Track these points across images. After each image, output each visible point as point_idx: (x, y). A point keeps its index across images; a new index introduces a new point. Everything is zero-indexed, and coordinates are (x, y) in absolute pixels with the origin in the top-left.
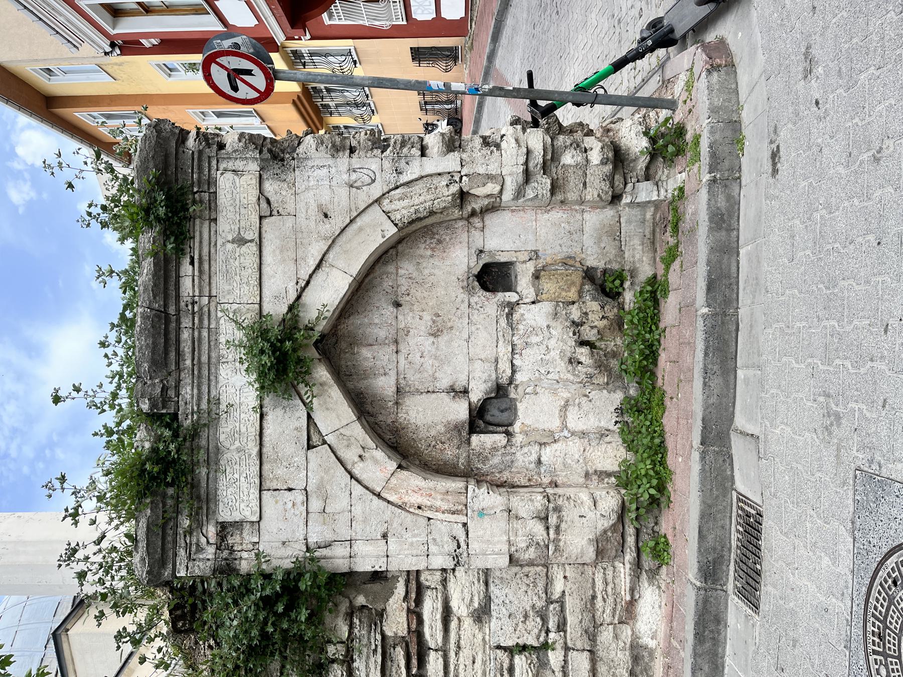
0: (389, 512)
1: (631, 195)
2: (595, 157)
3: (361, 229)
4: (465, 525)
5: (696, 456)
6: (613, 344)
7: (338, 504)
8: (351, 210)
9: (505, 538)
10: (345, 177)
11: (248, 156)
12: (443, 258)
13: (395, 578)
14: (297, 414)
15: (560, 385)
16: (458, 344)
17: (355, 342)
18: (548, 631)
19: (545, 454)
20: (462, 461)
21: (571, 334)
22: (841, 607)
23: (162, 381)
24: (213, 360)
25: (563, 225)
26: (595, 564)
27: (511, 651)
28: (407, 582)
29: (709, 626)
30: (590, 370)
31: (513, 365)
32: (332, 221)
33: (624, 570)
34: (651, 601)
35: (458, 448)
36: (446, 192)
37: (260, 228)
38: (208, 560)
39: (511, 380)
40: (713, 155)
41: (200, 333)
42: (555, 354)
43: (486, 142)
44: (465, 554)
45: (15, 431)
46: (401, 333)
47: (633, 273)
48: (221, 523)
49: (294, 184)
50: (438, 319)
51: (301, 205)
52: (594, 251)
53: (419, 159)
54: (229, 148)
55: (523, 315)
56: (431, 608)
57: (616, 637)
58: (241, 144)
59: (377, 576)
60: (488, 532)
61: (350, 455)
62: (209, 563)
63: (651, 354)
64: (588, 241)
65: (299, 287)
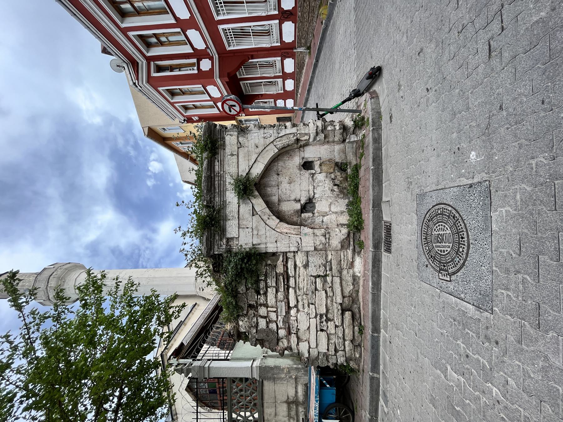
2: (337, 128)
3: (267, 151)
5: (371, 211)
7: (262, 232)
13: (279, 255)
17: (266, 186)
18: (327, 271)
22: (414, 237)
26: (341, 250)
27: (316, 277)
28: (283, 256)
29: (377, 263)
33: (350, 252)
34: (358, 262)
36: (293, 139)
39: (314, 197)
40: (373, 122)
42: (327, 188)
43: (304, 124)
45: (149, 259)
47: (350, 163)
51: (250, 144)
54: (228, 128)
56: (290, 264)
57: (348, 273)
59: (274, 254)
61: (265, 218)
63: (356, 187)
64: (336, 154)
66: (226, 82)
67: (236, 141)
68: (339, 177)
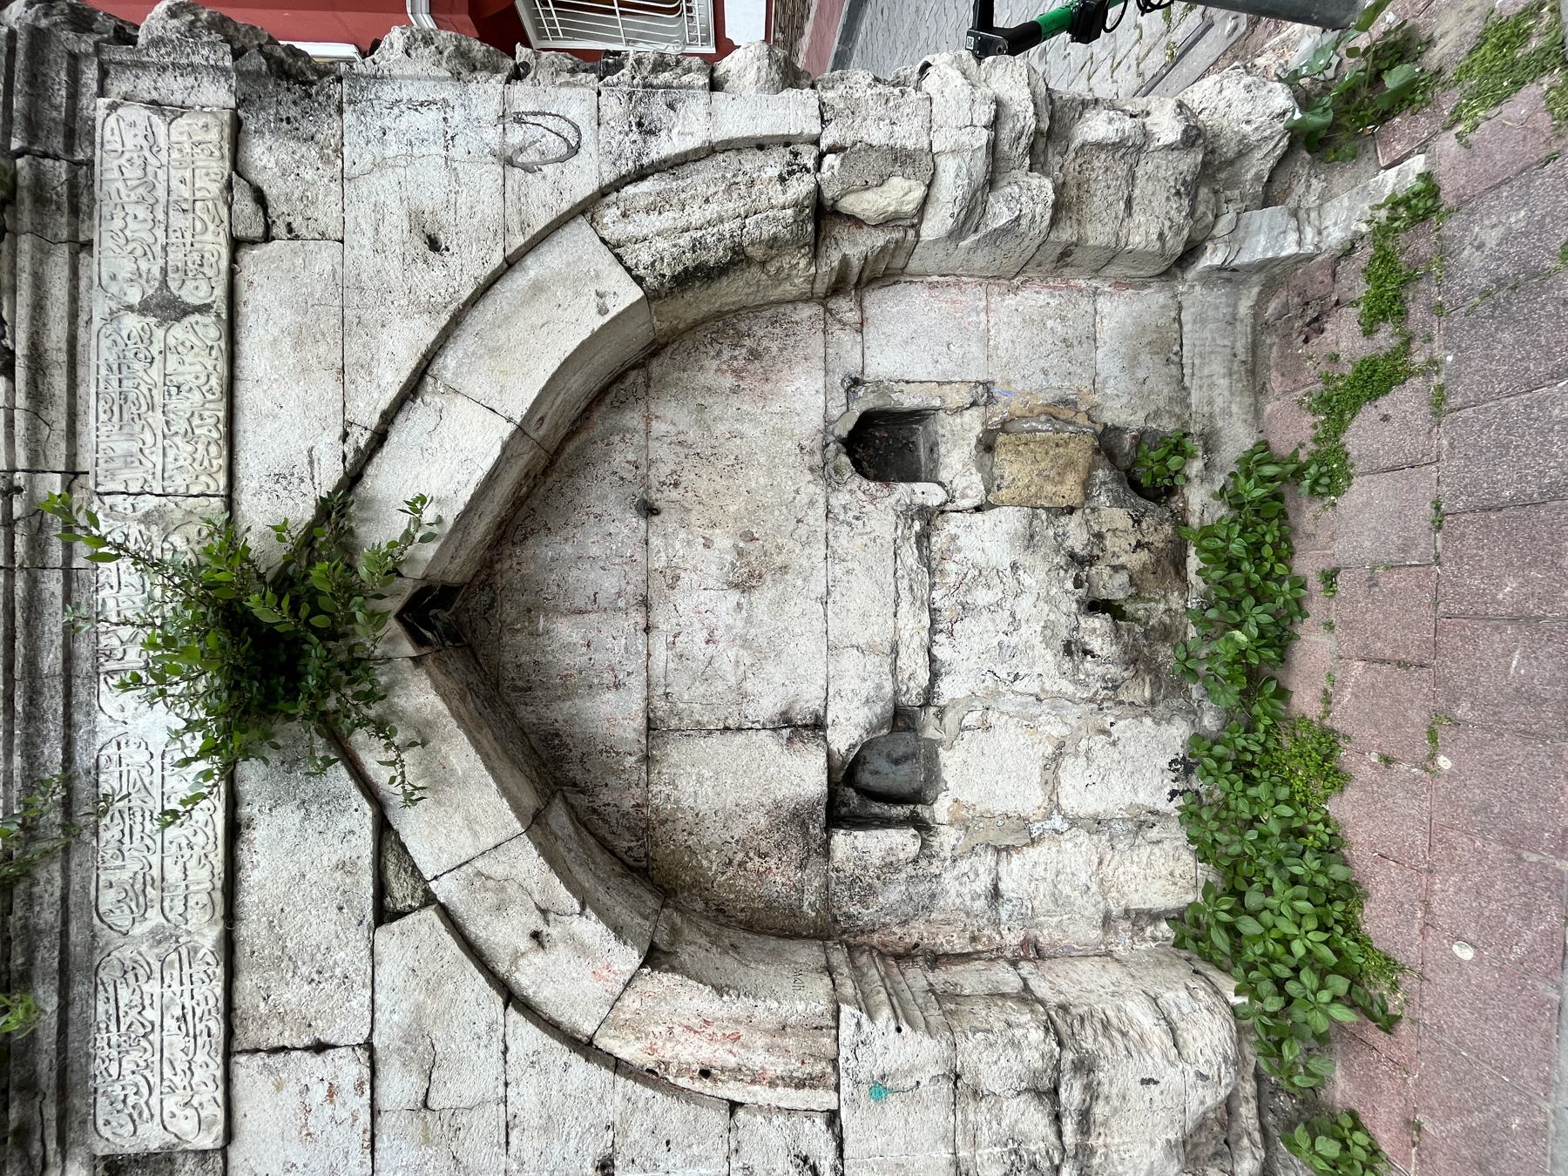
0: (618, 1099)
1: (1228, 243)
3: (537, 288)
6: (1162, 607)
7: (468, 1081)
9: (945, 1154)
10: (492, 136)
11: (196, 59)
12: (763, 397)
14: (344, 823)
15: (1045, 707)
16: (801, 612)
19: (1010, 874)
20: (809, 898)
21: (1069, 585)
24: (84, 666)
25: (1050, 323)
30: (1113, 669)
31: (932, 659)
32: (453, 261)
35: (802, 866)
36: (777, 197)
37: (232, 273)
39: (929, 695)
41: (33, 583)
42: (1030, 633)
46: (658, 582)
47: (1210, 442)
48: (104, 1158)
49: (338, 151)
50: (751, 546)
51: (360, 214)
52: (1122, 386)
53: (704, 96)
55: (954, 538)
58: (175, 22)
60: (899, 1141)
61: (503, 934)
64: (1107, 362)
65: (349, 448)
67: (212, 169)
68: (1119, 547)
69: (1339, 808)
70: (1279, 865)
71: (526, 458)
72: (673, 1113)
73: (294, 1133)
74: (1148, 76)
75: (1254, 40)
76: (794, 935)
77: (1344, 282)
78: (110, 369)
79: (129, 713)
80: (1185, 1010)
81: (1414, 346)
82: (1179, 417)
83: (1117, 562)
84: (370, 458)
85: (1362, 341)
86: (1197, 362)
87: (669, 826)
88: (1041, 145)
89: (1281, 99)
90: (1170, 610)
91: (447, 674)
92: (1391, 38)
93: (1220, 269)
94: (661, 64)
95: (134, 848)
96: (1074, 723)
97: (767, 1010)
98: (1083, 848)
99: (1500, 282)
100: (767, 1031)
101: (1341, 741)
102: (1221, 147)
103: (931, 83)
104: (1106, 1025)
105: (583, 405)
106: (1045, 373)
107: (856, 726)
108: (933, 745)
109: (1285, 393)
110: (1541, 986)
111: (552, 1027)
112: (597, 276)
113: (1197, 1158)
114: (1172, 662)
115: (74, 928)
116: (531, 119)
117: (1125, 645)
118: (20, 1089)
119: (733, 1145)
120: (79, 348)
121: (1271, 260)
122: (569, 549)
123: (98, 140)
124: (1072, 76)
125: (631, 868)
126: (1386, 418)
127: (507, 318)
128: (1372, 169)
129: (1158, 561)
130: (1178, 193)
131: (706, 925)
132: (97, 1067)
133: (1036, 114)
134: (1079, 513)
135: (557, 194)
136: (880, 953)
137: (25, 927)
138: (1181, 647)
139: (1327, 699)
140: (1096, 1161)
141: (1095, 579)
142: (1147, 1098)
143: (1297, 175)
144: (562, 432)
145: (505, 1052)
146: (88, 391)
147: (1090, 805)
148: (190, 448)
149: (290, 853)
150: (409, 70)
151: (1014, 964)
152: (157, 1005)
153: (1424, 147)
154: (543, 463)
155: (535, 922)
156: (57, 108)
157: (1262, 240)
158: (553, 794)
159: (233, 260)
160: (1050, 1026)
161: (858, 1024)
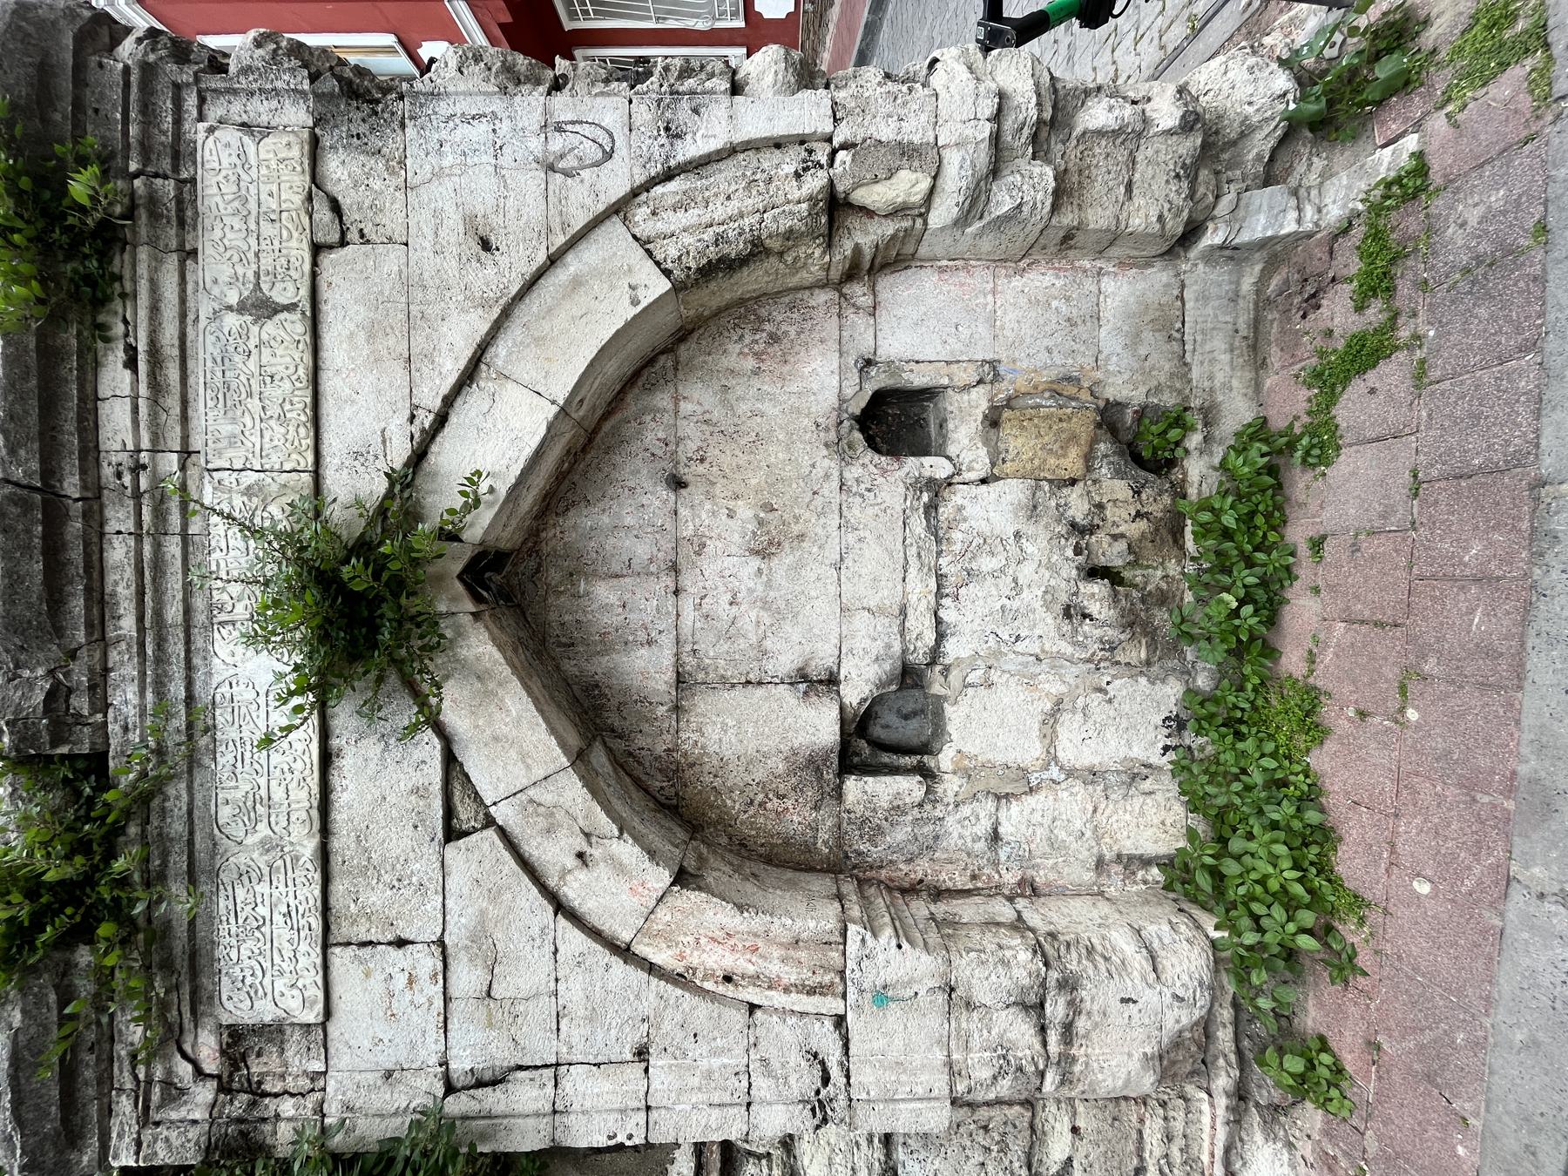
0: (652, 997)
3: (577, 283)
4: (840, 1021)
6: (1159, 573)
7: (525, 975)
8: (549, 230)
9: (939, 1056)
11: (279, 84)
14: (417, 755)
17: (579, 569)
20: (823, 835)
21: (1070, 553)
23: (51, 673)
24: (200, 618)
25: (1054, 304)
30: (1110, 632)
31: (939, 622)
32: (503, 260)
35: (816, 808)
36: (792, 191)
37: (314, 275)
38: (195, 1122)
39: (935, 654)
41: (158, 547)
42: (1032, 597)
44: (842, 1101)
46: (686, 550)
47: (1209, 415)
48: (228, 1027)
49: (402, 163)
50: (770, 516)
51: (422, 219)
53: (725, 100)
55: (960, 509)
58: (260, 52)
60: (898, 1042)
61: (553, 854)
62: (193, 1133)
64: (1110, 341)
66: (502, 26)
68: (1120, 517)
69: (1319, 760)
70: (1260, 812)
71: (568, 436)
72: (701, 1011)
73: (381, 1014)
74: (1170, 49)
75: (1266, 16)
76: (810, 869)
77: (1340, 260)
78: (215, 361)
79: (238, 658)
80: (1166, 941)
81: (1400, 322)
82: (1179, 392)
83: (1117, 531)
84: (433, 437)
85: (1355, 317)
86: (1199, 338)
87: (697, 769)
88: (1044, 134)
89: (1282, 81)
90: (1167, 576)
91: (502, 628)
92: (1391, 18)
93: (1222, 247)
94: (686, 72)
95: (245, 771)
96: (1072, 681)
97: (782, 926)
98: (1079, 797)
99: (1479, 259)
100: (781, 944)
101: (1322, 698)
102: (1224, 128)
103: (937, 80)
104: (1090, 951)
105: (618, 387)
106: (1049, 351)
107: (867, 681)
108: (940, 700)
109: (1283, 367)
110: (1487, 914)
111: (595, 934)
112: (630, 270)
113: (1175, 1075)
114: (1169, 625)
115: (198, 837)
116: (569, 127)
117: (1123, 609)
118: (161, 968)
119: (752, 1040)
120: (189, 344)
121: (1271, 238)
122: (606, 519)
123: (199, 159)
124: (1096, 48)
125: (663, 805)
126: (1372, 391)
127: (550, 310)
128: (1370, 148)
129: (1157, 530)
130: (1177, 176)
131: (728, 856)
132: (220, 952)
133: (1039, 104)
134: (1081, 484)
135: (593, 196)
136: (887, 887)
137: (160, 835)
138: (1176, 611)
139: (1311, 658)
140: (1077, 1068)
141: (1094, 547)
142: (1126, 1015)
143: (1299, 154)
144: (599, 412)
145: (556, 952)
146: (197, 380)
147: (1087, 757)
148: (283, 430)
149: (373, 779)
150: (462, 87)
151: (1011, 899)
152: (267, 902)
153: (1418, 126)
154: (582, 440)
155: (580, 844)
156: (164, 133)
157: (1262, 219)
158: (594, 738)
159: (315, 264)
160: (1038, 949)
161: (863, 940)
